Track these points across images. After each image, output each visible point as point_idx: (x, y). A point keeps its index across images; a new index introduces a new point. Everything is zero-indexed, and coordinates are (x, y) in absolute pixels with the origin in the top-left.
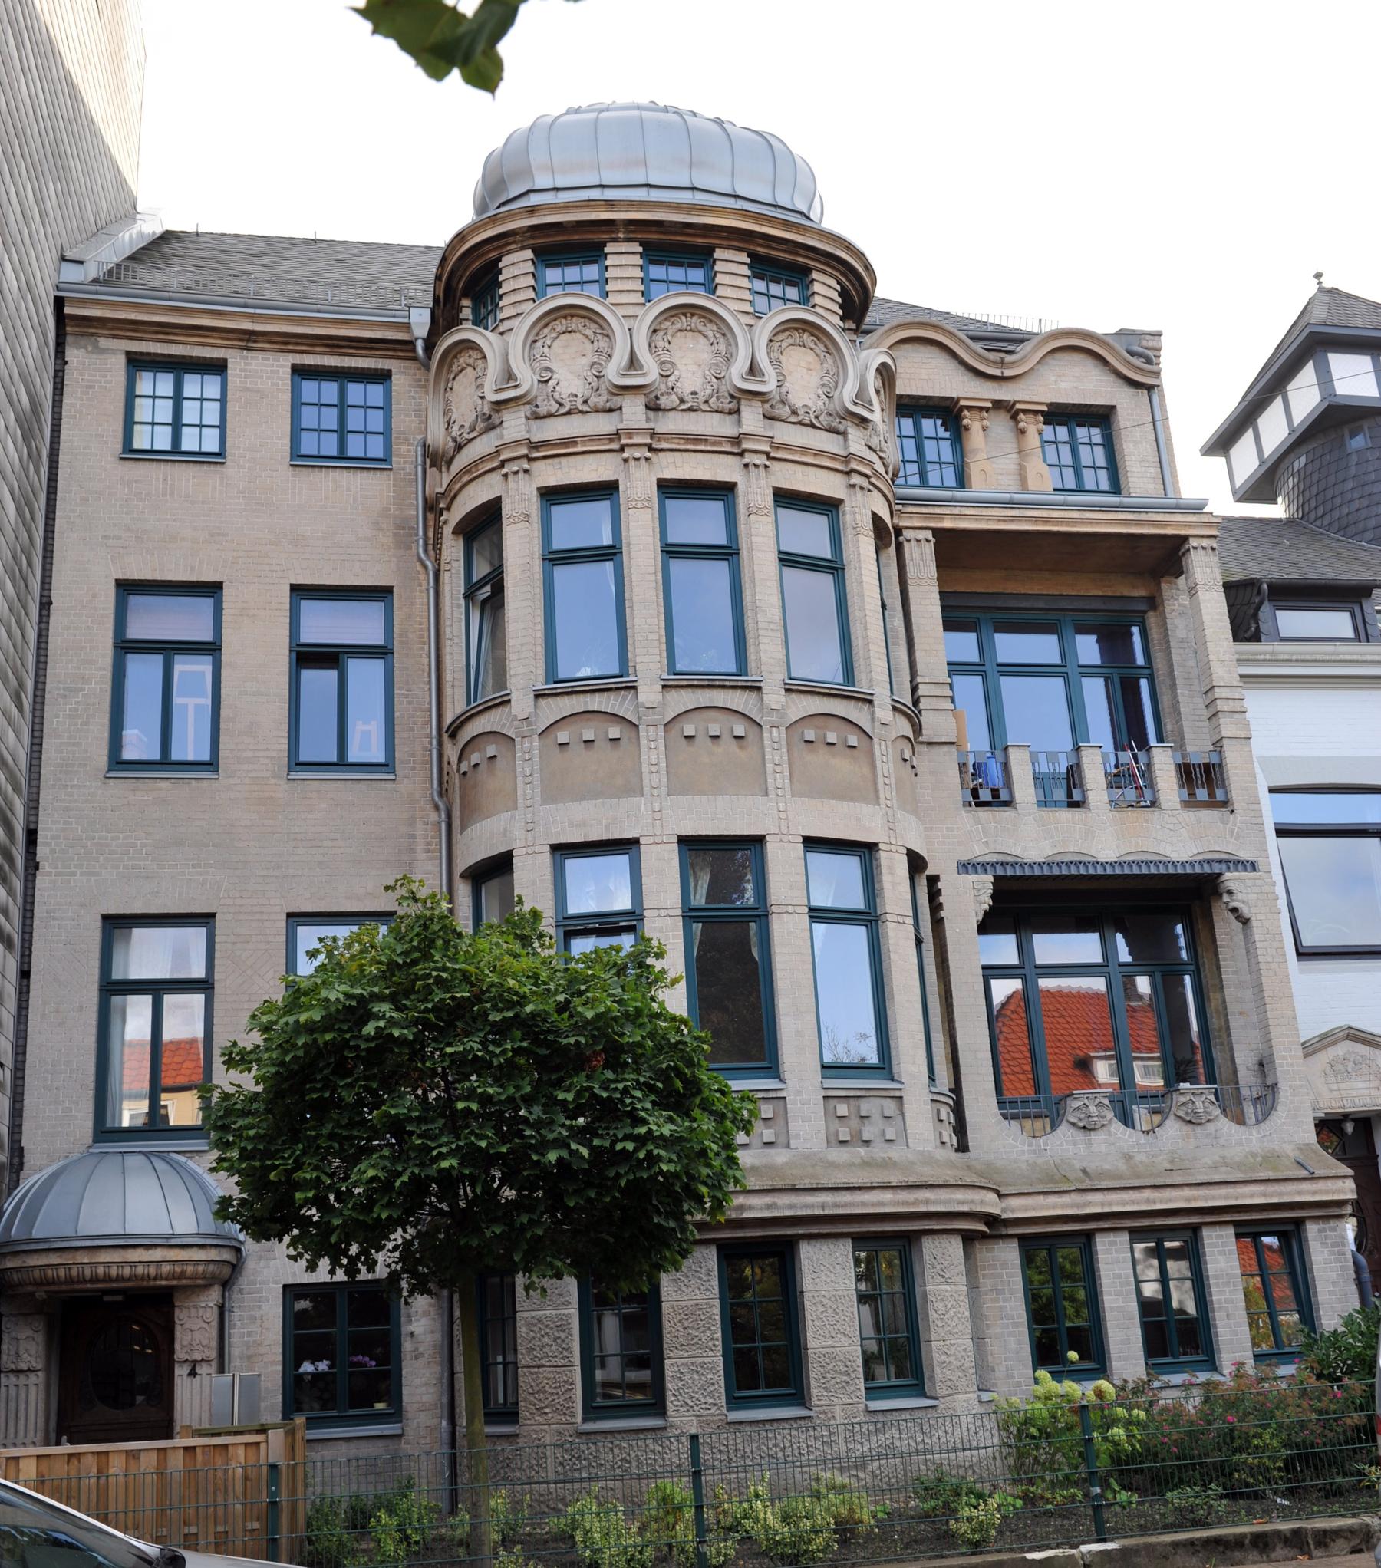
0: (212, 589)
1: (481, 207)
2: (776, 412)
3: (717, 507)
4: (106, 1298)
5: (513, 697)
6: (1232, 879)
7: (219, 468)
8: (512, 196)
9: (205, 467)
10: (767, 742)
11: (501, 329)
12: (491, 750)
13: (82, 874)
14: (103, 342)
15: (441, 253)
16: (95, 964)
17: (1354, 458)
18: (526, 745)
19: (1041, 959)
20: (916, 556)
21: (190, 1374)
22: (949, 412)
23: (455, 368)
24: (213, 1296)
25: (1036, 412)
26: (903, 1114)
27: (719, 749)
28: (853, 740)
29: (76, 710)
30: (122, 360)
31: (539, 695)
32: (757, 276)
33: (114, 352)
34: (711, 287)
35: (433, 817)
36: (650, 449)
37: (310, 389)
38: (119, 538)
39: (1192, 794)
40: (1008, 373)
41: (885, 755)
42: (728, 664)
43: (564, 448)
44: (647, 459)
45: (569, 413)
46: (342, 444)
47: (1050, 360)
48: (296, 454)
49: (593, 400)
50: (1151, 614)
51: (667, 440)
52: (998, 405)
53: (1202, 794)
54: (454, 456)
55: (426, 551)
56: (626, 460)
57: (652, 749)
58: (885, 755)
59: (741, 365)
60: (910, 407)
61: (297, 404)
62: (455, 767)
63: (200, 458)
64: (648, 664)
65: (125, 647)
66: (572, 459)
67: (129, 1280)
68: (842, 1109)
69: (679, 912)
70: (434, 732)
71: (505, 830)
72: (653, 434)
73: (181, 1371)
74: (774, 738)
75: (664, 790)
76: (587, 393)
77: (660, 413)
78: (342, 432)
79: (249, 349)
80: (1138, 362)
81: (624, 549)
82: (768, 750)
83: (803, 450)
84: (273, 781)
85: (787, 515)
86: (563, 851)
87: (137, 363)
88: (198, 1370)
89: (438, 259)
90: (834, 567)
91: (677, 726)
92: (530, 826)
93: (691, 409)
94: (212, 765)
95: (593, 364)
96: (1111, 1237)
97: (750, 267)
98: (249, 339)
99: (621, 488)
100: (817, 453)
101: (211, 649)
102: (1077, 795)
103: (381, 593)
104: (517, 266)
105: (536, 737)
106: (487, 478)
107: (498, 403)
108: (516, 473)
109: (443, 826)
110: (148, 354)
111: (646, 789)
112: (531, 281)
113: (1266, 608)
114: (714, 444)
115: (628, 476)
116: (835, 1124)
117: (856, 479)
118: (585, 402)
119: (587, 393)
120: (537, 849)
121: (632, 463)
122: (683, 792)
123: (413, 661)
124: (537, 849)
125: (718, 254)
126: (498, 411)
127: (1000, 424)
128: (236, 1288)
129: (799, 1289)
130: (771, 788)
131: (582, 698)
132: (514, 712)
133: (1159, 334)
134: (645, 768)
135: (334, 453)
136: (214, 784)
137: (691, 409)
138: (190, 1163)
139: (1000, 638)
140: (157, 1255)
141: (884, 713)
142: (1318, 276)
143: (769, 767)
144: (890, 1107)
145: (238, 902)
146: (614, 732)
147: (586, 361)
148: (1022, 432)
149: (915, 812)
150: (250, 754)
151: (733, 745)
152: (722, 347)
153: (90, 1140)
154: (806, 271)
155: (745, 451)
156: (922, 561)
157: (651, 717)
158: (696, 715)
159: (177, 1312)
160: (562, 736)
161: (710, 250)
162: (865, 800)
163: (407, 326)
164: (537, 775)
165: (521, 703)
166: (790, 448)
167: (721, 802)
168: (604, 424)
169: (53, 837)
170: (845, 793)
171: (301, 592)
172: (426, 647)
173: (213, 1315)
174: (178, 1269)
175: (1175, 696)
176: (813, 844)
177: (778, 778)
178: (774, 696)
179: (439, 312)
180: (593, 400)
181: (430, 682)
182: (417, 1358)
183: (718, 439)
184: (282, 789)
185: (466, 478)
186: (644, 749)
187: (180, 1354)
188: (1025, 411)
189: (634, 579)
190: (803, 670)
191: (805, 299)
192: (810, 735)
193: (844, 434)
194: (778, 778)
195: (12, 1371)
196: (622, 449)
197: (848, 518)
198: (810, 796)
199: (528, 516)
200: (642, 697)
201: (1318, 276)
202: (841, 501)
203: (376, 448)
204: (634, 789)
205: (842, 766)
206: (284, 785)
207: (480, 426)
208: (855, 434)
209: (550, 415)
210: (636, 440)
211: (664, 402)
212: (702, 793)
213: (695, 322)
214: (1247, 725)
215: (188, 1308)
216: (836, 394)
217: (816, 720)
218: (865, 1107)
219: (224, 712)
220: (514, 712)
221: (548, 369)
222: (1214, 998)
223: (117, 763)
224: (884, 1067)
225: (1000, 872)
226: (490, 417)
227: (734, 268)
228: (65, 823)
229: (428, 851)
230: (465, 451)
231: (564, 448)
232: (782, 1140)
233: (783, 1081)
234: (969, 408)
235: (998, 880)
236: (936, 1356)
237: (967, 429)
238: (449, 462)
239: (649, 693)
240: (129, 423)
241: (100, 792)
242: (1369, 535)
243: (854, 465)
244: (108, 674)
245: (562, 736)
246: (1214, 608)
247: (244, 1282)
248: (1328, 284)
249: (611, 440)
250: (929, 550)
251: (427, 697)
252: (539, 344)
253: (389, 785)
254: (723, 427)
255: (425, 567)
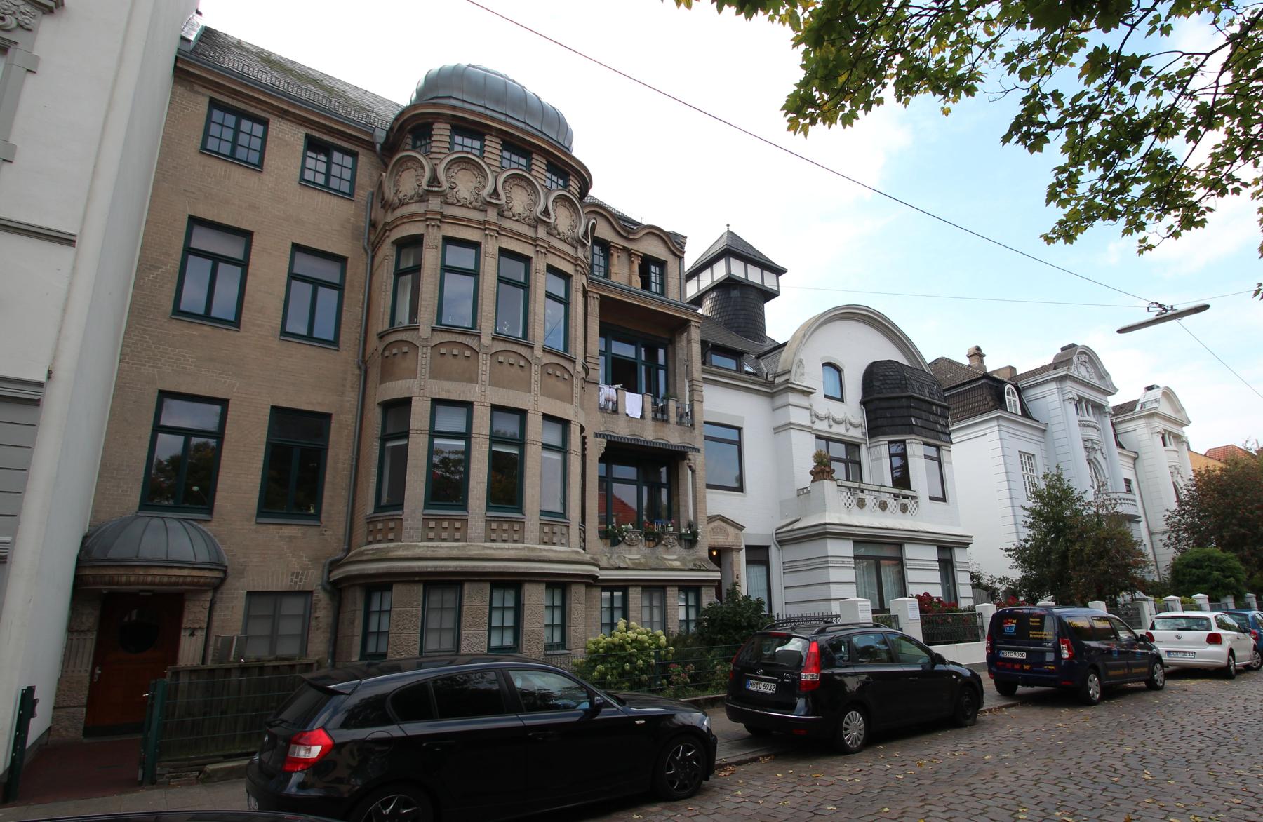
0: (247, 235)
1: (420, 93)
2: (551, 232)
3: (472, 252)
4: (141, 594)
5: (421, 327)
6: (691, 455)
7: (258, 173)
8: (440, 95)
9: (250, 171)
10: (533, 371)
11: (431, 156)
12: (405, 349)
13: (149, 366)
14: (197, 88)
15: (400, 109)
16: (152, 415)
17: (733, 300)
18: (425, 350)
19: (615, 475)
20: (592, 304)
21: (190, 635)
22: (605, 246)
23: (404, 167)
24: (209, 596)
25: (638, 256)
26: (568, 533)
27: (512, 370)
28: (566, 376)
29: (156, 278)
30: (207, 100)
31: (433, 330)
32: (548, 170)
33: (203, 95)
34: (529, 170)
35: (357, 372)
36: (498, 233)
37: (217, 115)
38: (194, 193)
39: (656, 415)
40: (631, 237)
41: (577, 383)
42: (468, 324)
43: (457, 222)
44: (496, 237)
45: (462, 206)
46: (233, 150)
47: (645, 237)
48: (302, 179)
49: (474, 203)
50: (670, 346)
51: (506, 231)
52: (625, 249)
53: (659, 416)
54: (398, 207)
55: (368, 244)
56: (486, 235)
57: (484, 365)
58: (577, 383)
59: (540, 208)
60: (598, 242)
61: (209, 121)
62: (380, 352)
63: (246, 164)
64: (486, 328)
65: (189, 251)
66: (461, 227)
67: (181, 585)
68: (546, 529)
69: (428, 432)
70: (363, 332)
71: (409, 388)
72: (500, 227)
73: (185, 634)
74: (535, 369)
75: (487, 383)
76: (472, 199)
77: (503, 219)
78: (235, 143)
79: (283, 118)
80: (678, 246)
81: (481, 274)
82: (533, 374)
83: (561, 251)
84: (271, 338)
85: (551, 276)
86: (436, 402)
87: (214, 104)
88: (196, 633)
89: (397, 112)
90: (565, 302)
91: (495, 357)
92: (422, 388)
93: (517, 220)
94: (236, 323)
95: (476, 188)
96: (634, 589)
97: (546, 166)
98: (284, 114)
99: (483, 246)
100: (566, 253)
101: (244, 264)
102: (665, 417)
103: (341, 260)
104: (441, 132)
105: (429, 348)
106: (417, 224)
107: (428, 191)
108: (433, 226)
109: (363, 377)
110: (224, 102)
111: (479, 381)
112: (448, 139)
113: (709, 352)
114: (525, 238)
115: (486, 241)
116: (543, 535)
117: (579, 268)
118: (470, 203)
119: (472, 199)
120: (425, 399)
121: (489, 237)
122: (433, 379)
123: (355, 296)
124: (425, 399)
125: (534, 156)
126: (427, 195)
127: (624, 256)
128: (219, 592)
129: (522, 603)
130: (532, 391)
131: (454, 335)
132: (420, 334)
133: (686, 238)
134: (480, 372)
135: (228, 153)
136: (238, 333)
137: (517, 220)
138: (200, 526)
139: (614, 343)
140: (185, 572)
141: (579, 368)
142: (728, 225)
143: (533, 381)
144: (564, 530)
145: (244, 395)
146: (468, 353)
147: (473, 185)
148: (633, 262)
149: (583, 409)
150: (259, 322)
151: (519, 370)
152: (533, 197)
153: (136, 508)
154: (568, 175)
155: (538, 245)
156: (595, 307)
157: (485, 350)
158: (505, 353)
159: (187, 603)
160: (443, 350)
161: (531, 153)
162: (568, 403)
163: (372, 135)
164: (428, 365)
165: (425, 331)
166: (556, 249)
167: (512, 393)
168: (478, 216)
169: (133, 343)
170: (559, 397)
171: (297, 248)
172: (363, 291)
173: (207, 605)
174: (196, 580)
175: (675, 380)
176: (547, 417)
177: (536, 387)
178: (538, 352)
179: (391, 135)
180: (474, 203)
181: (363, 308)
182: (317, 629)
183: (527, 237)
184: (275, 343)
185: (405, 220)
186: (480, 364)
187: (185, 624)
188: (635, 254)
189: (485, 288)
190: (550, 344)
191: (566, 186)
192: (550, 371)
193: (576, 248)
194: (536, 387)
195: (77, 631)
196: (485, 229)
197: (574, 283)
198: (547, 396)
199: (437, 247)
200: (482, 341)
201: (728, 225)
202: (572, 276)
203: (345, 187)
204: (473, 379)
205: (561, 386)
206: (277, 341)
207: (416, 198)
208: (580, 249)
209: (453, 204)
210: (492, 227)
211: (506, 213)
212: (503, 387)
213: (523, 183)
214: (702, 396)
215: (199, 600)
216: (576, 231)
217: (553, 365)
218: (556, 529)
219: (247, 298)
220: (420, 334)
221: (454, 183)
222: (675, 499)
223: (177, 312)
224: (563, 515)
225: (609, 438)
226: (422, 196)
227: (493, 145)
228: (142, 337)
229: (352, 387)
230: (405, 207)
231: (457, 222)
232: (521, 539)
233: (524, 515)
234: (614, 247)
235: (609, 442)
236: (573, 633)
237: (612, 255)
238: (394, 209)
239: (486, 339)
240: (206, 135)
241: (166, 324)
242: (734, 329)
243: (579, 262)
244: (179, 263)
245: (443, 350)
246: (696, 349)
247: (225, 588)
248: (731, 229)
249: (480, 224)
250: (597, 303)
251: (360, 313)
252: (452, 170)
253: (335, 352)
254: (529, 232)
255: (367, 253)
